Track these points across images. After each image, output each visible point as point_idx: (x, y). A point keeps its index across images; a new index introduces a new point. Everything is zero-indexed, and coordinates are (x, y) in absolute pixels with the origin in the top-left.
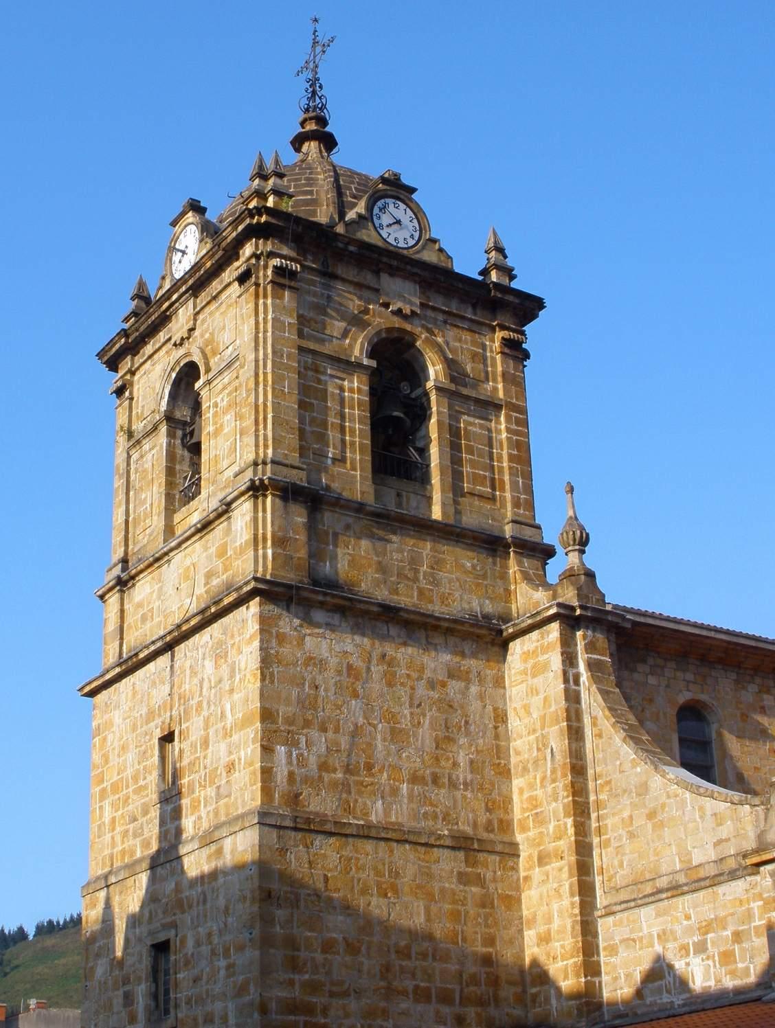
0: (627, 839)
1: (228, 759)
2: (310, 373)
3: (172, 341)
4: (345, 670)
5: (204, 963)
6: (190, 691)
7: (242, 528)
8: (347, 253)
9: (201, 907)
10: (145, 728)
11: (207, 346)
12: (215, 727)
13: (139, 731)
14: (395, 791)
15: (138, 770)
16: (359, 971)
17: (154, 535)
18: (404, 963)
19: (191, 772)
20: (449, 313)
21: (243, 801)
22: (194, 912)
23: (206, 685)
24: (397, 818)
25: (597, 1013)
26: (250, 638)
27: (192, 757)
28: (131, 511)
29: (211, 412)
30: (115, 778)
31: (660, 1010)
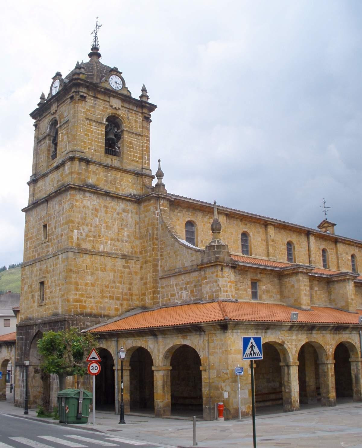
2: (89, 126)
5: (53, 288)
9: (53, 273)
14: (106, 243)
16: (95, 291)
18: (107, 289)
20: (129, 109)
22: (51, 273)
23: (56, 212)
24: (107, 250)
25: (158, 304)
30: (30, 236)
31: (174, 304)
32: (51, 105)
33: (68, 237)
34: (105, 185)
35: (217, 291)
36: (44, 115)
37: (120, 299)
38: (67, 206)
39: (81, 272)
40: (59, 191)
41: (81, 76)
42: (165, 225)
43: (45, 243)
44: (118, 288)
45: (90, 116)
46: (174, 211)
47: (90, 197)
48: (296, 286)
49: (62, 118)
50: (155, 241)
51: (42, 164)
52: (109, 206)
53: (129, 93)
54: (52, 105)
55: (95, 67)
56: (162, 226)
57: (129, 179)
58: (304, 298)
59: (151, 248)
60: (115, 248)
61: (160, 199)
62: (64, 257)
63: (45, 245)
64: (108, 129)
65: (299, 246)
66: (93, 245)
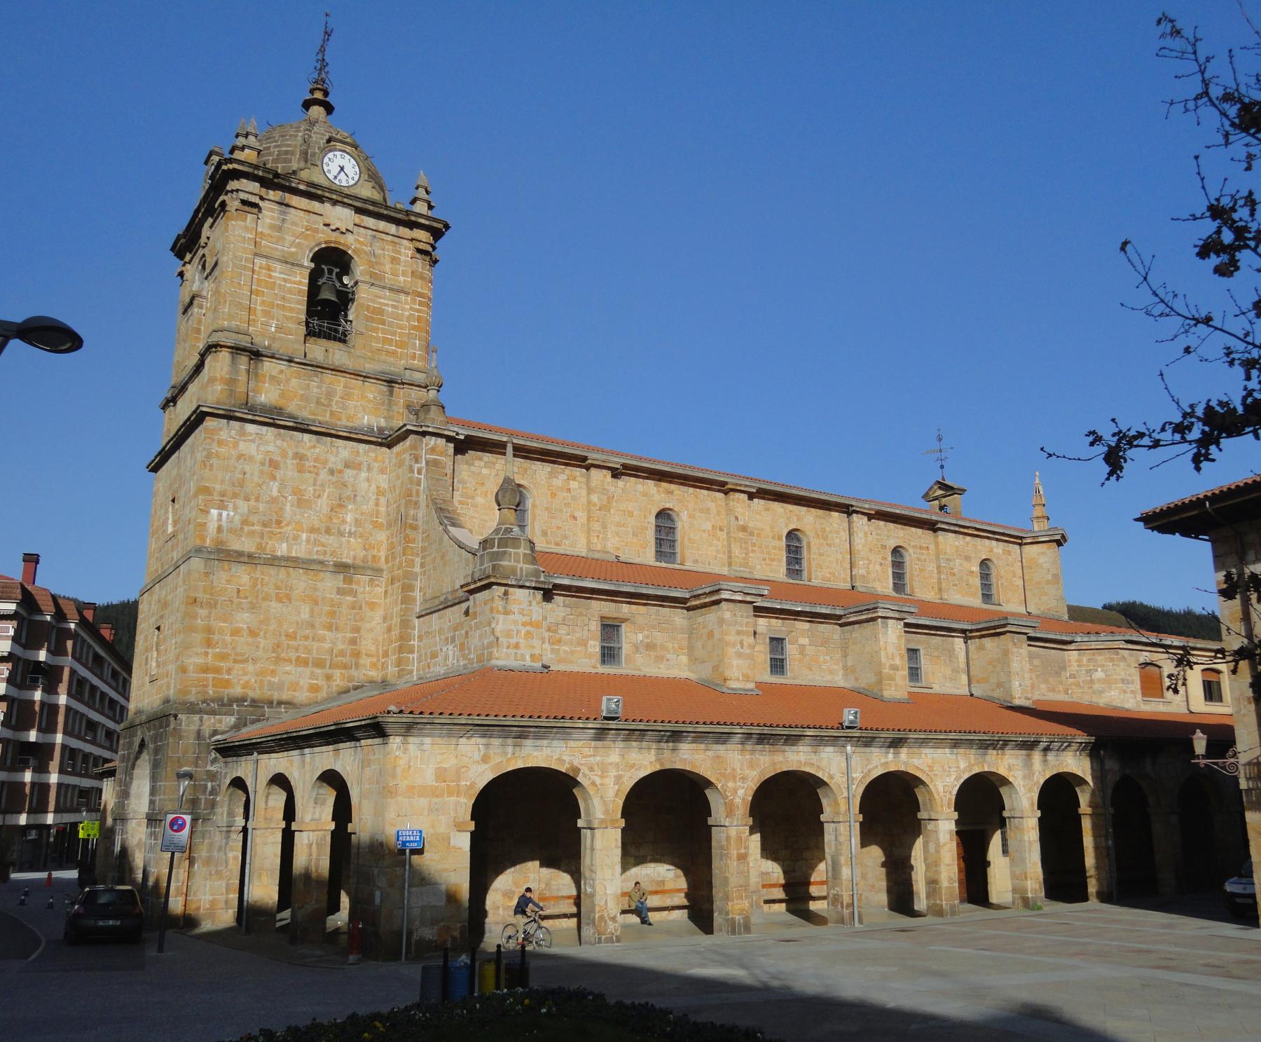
14: (296, 538)
18: (291, 643)
24: (296, 553)
35: (490, 645)
37: (325, 665)
39: (222, 604)
44: (322, 640)
48: (717, 636)
57: (373, 391)
58: (736, 662)
60: (319, 548)
65: (822, 541)
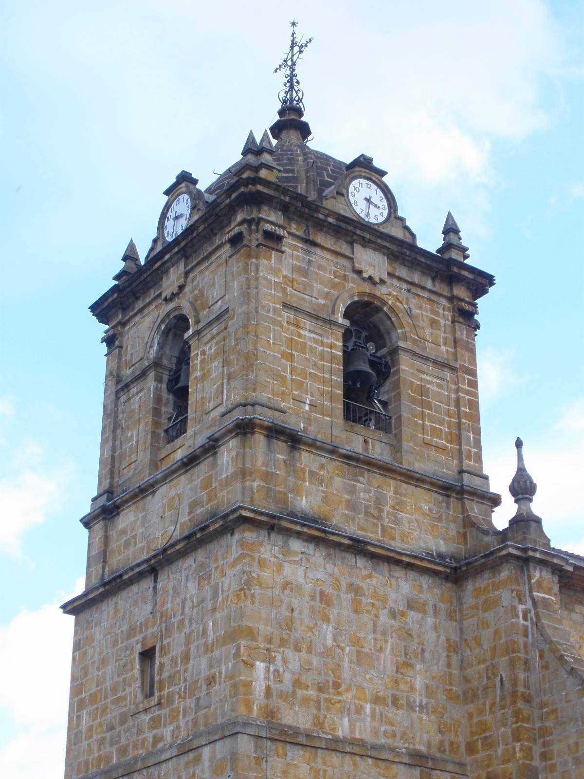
0: (573, 765)
1: (208, 673)
2: (292, 328)
3: (163, 296)
4: (318, 595)
6: (172, 610)
7: (228, 462)
8: (326, 224)
10: (125, 643)
11: (196, 301)
12: (196, 644)
13: (120, 646)
14: (359, 710)
15: (117, 683)
17: (139, 469)
19: (171, 684)
20: (412, 283)
21: (223, 711)
23: (188, 604)
24: (360, 734)
26: (234, 561)
27: (173, 671)
28: (117, 447)
29: (199, 359)
30: (94, 689)
32: (163, 271)
33: (235, 686)
34: (347, 519)
36: (140, 304)
38: (229, 582)
40: (198, 536)
41: (263, 173)
42: (553, 651)
43: (146, 710)
45: (295, 299)
46: (573, 610)
47: (303, 553)
49: (204, 309)
50: (520, 704)
51: (134, 457)
52: (365, 586)
53: (407, 235)
54: (167, 271)
55: (300, 158)
56: (541, 656)
59: (510, 731)
61: (531, 565)
62: (219, 756)
63: (147, 717)
64: (350, 345)
66: (316, 717)
